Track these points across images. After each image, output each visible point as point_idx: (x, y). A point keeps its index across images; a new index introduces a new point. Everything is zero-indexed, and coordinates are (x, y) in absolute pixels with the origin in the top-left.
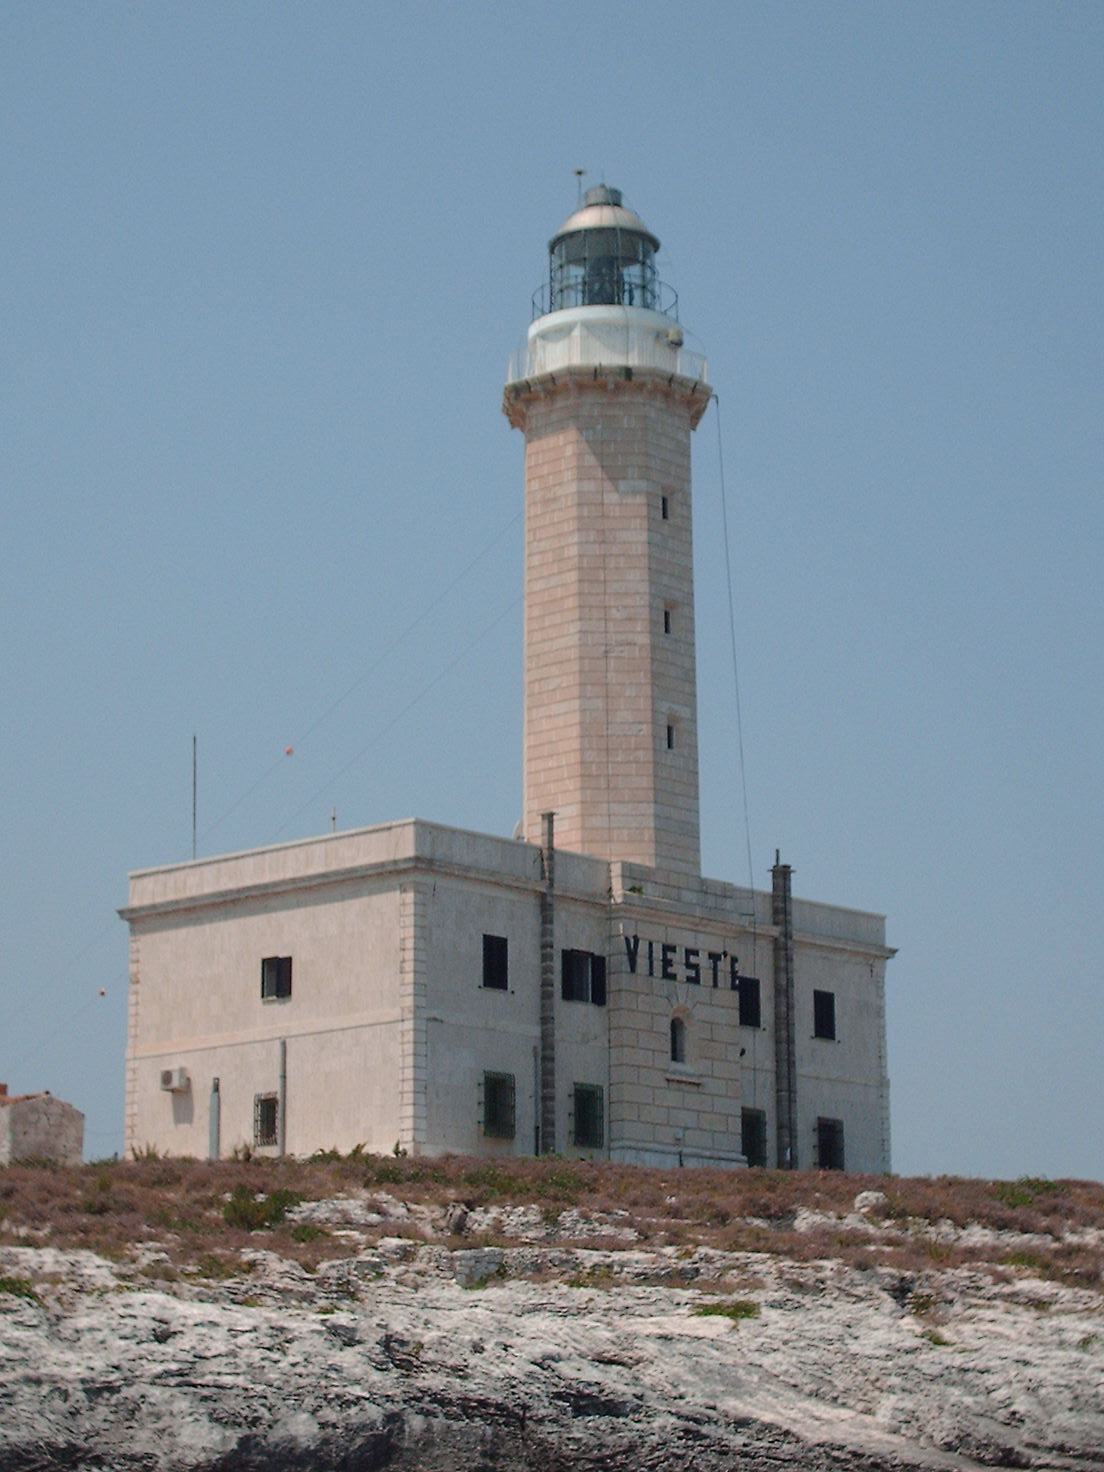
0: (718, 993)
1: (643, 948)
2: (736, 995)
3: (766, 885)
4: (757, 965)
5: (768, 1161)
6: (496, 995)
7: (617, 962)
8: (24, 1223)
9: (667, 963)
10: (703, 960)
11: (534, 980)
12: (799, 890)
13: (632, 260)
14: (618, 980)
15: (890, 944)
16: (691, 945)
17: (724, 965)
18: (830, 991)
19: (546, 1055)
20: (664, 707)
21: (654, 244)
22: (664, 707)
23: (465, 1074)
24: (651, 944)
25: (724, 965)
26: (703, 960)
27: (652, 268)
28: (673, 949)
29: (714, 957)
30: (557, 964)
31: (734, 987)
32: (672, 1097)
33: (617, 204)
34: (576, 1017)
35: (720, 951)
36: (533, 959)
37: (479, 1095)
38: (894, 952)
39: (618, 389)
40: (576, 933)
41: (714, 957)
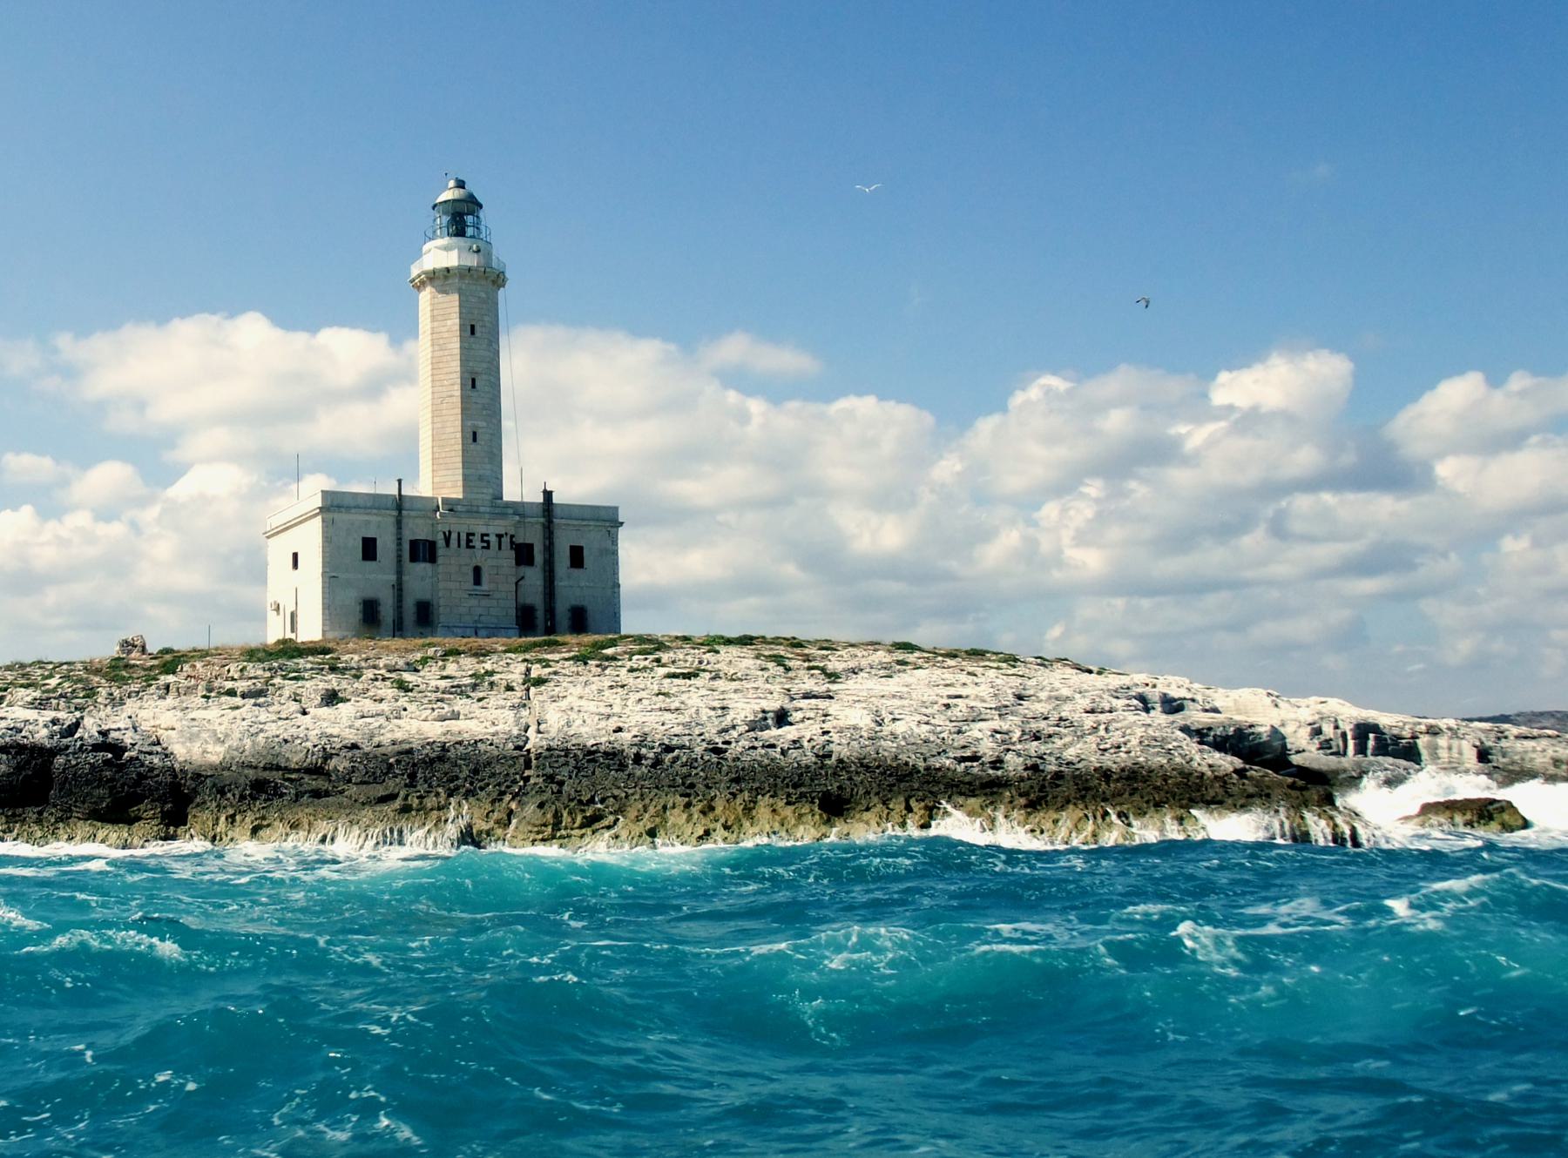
0: (501, 554)
1: (454, 536)
2: (513, 553)
3: (540, 499)
4: (534, 536)
5: (1423, 758)
6: (369, 564)
7: (441, 543)
8: (871, 936)
9: (469, 541)
10: (493, 539)
11: (392, 556)
12: (555, 500)
13: (471, 213)
14: (441, 550)
15: (620, 520)
16: (484, 531)
17: (506, 540)
18: (528, 541)
19: (399, 588)
20: (469, 423)
21: (480, 206)
22: (469, 423)
23: (351, 600)
24: (459, 534)
25: (506, 540)
26: (493, 539)
27: (478, 217)
28: (473, 534)
29: (500, 536)
30: (406, 547)
31: (512, 548)
32: (473, 602)
33: (464, 188)
34: (422, 568)
35: (503, 532)
36: (392, 546)
37: (359, 608)
38: (622, 523)
39: (446, 278)
40: (417, 529)
41: (500, 536)
